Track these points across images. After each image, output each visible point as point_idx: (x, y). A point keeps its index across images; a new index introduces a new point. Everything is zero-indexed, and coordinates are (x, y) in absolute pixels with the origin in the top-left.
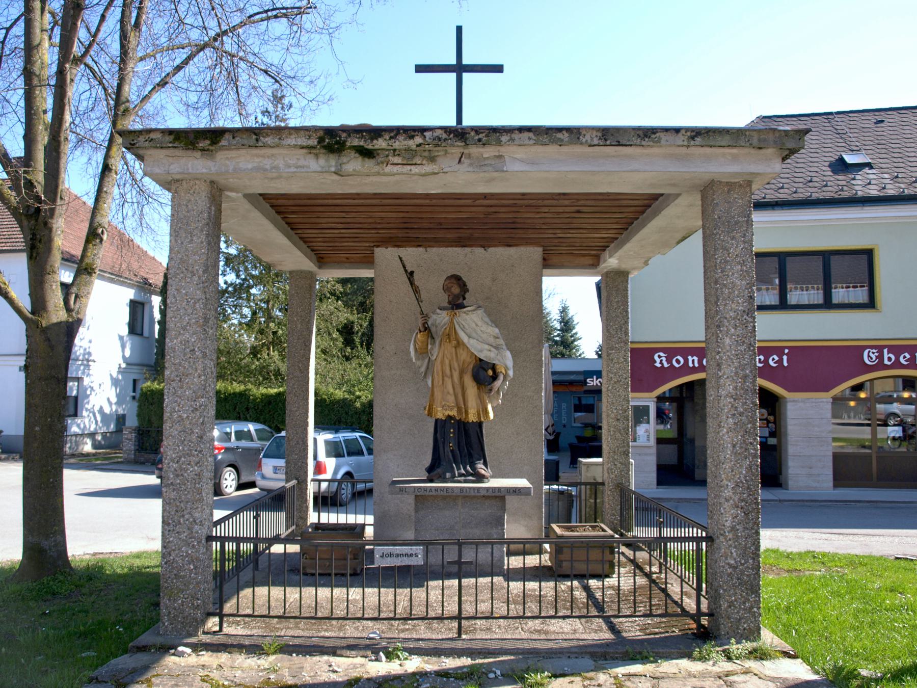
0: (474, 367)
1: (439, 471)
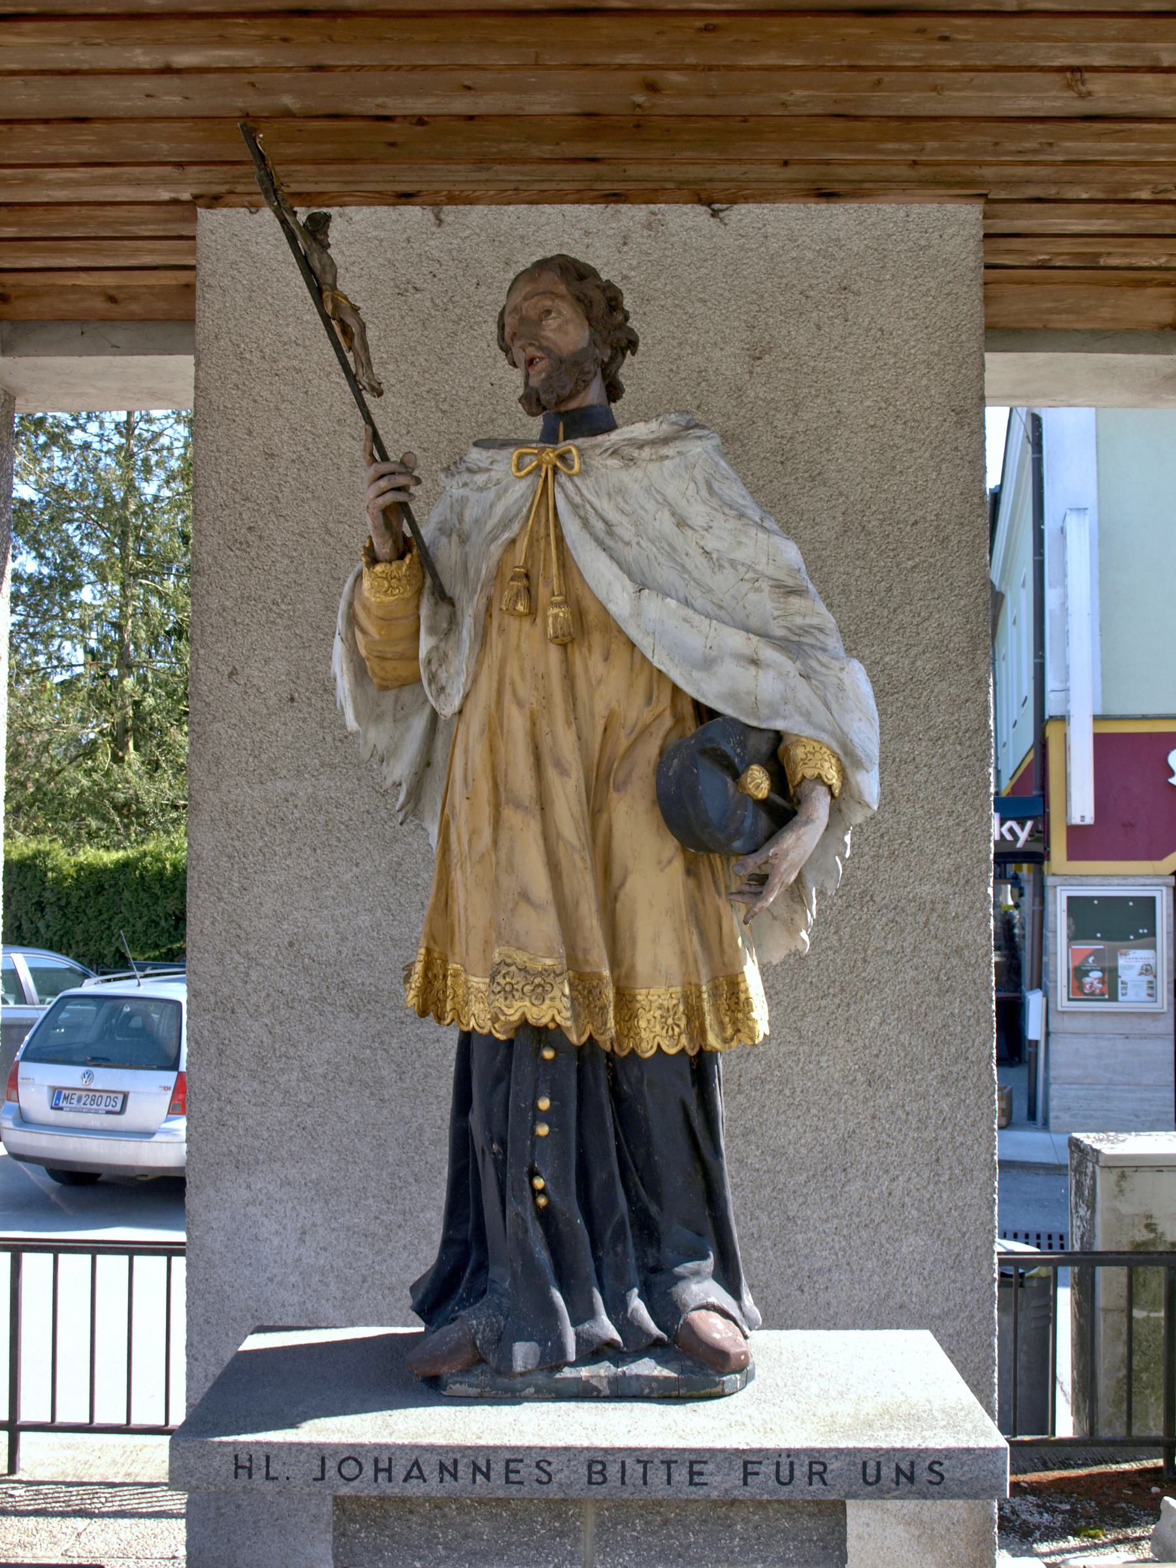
0: (664, 754)
1: (474, 1322)
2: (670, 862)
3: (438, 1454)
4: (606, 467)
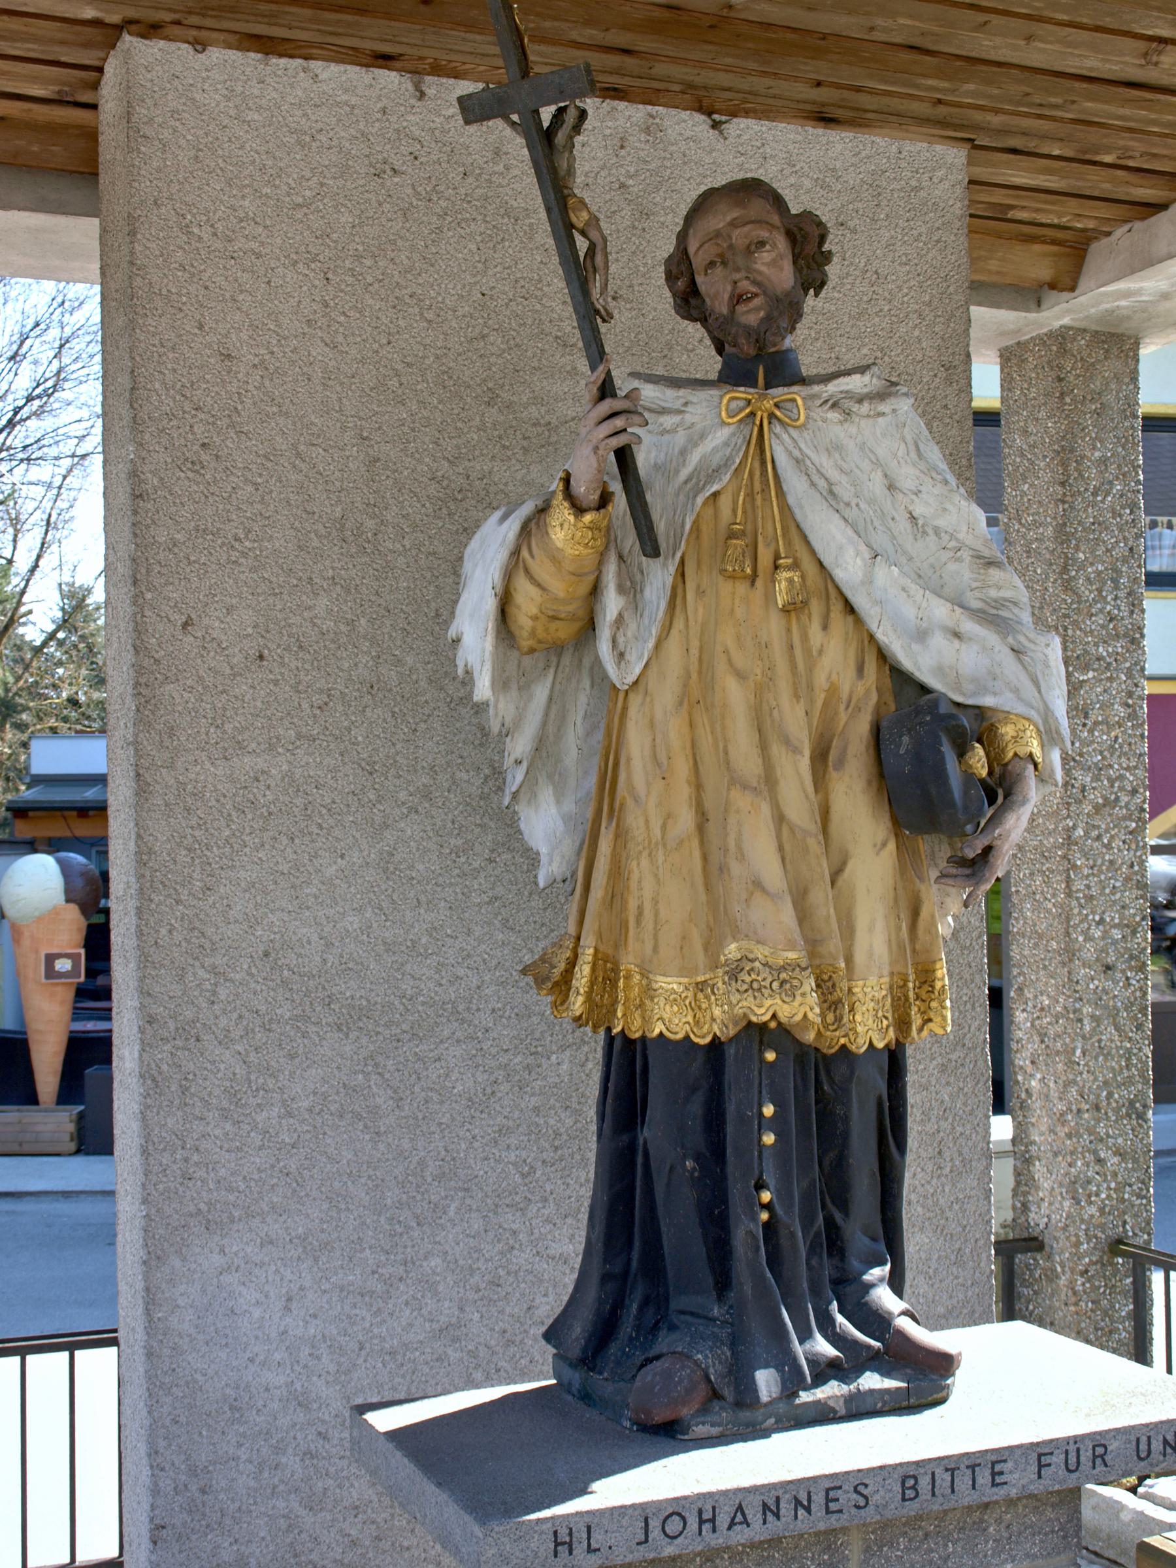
2: (884, 845)
3: (762, 1494)
4: (825, 420)
